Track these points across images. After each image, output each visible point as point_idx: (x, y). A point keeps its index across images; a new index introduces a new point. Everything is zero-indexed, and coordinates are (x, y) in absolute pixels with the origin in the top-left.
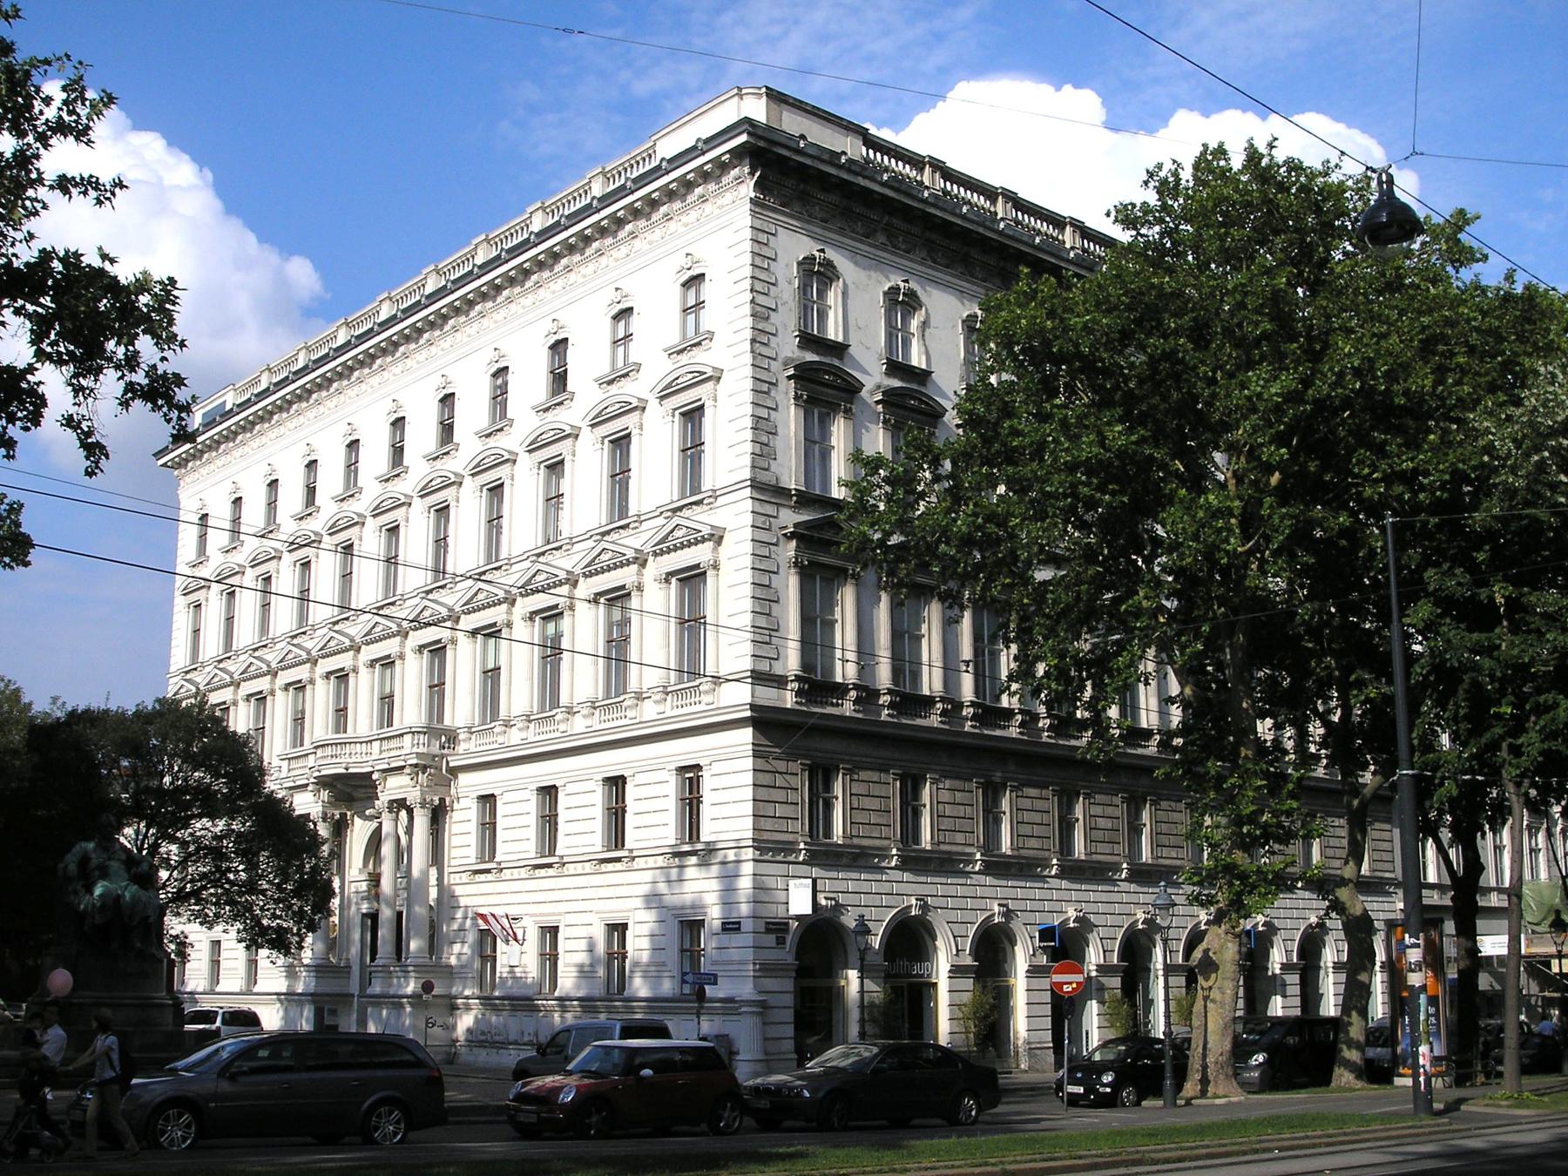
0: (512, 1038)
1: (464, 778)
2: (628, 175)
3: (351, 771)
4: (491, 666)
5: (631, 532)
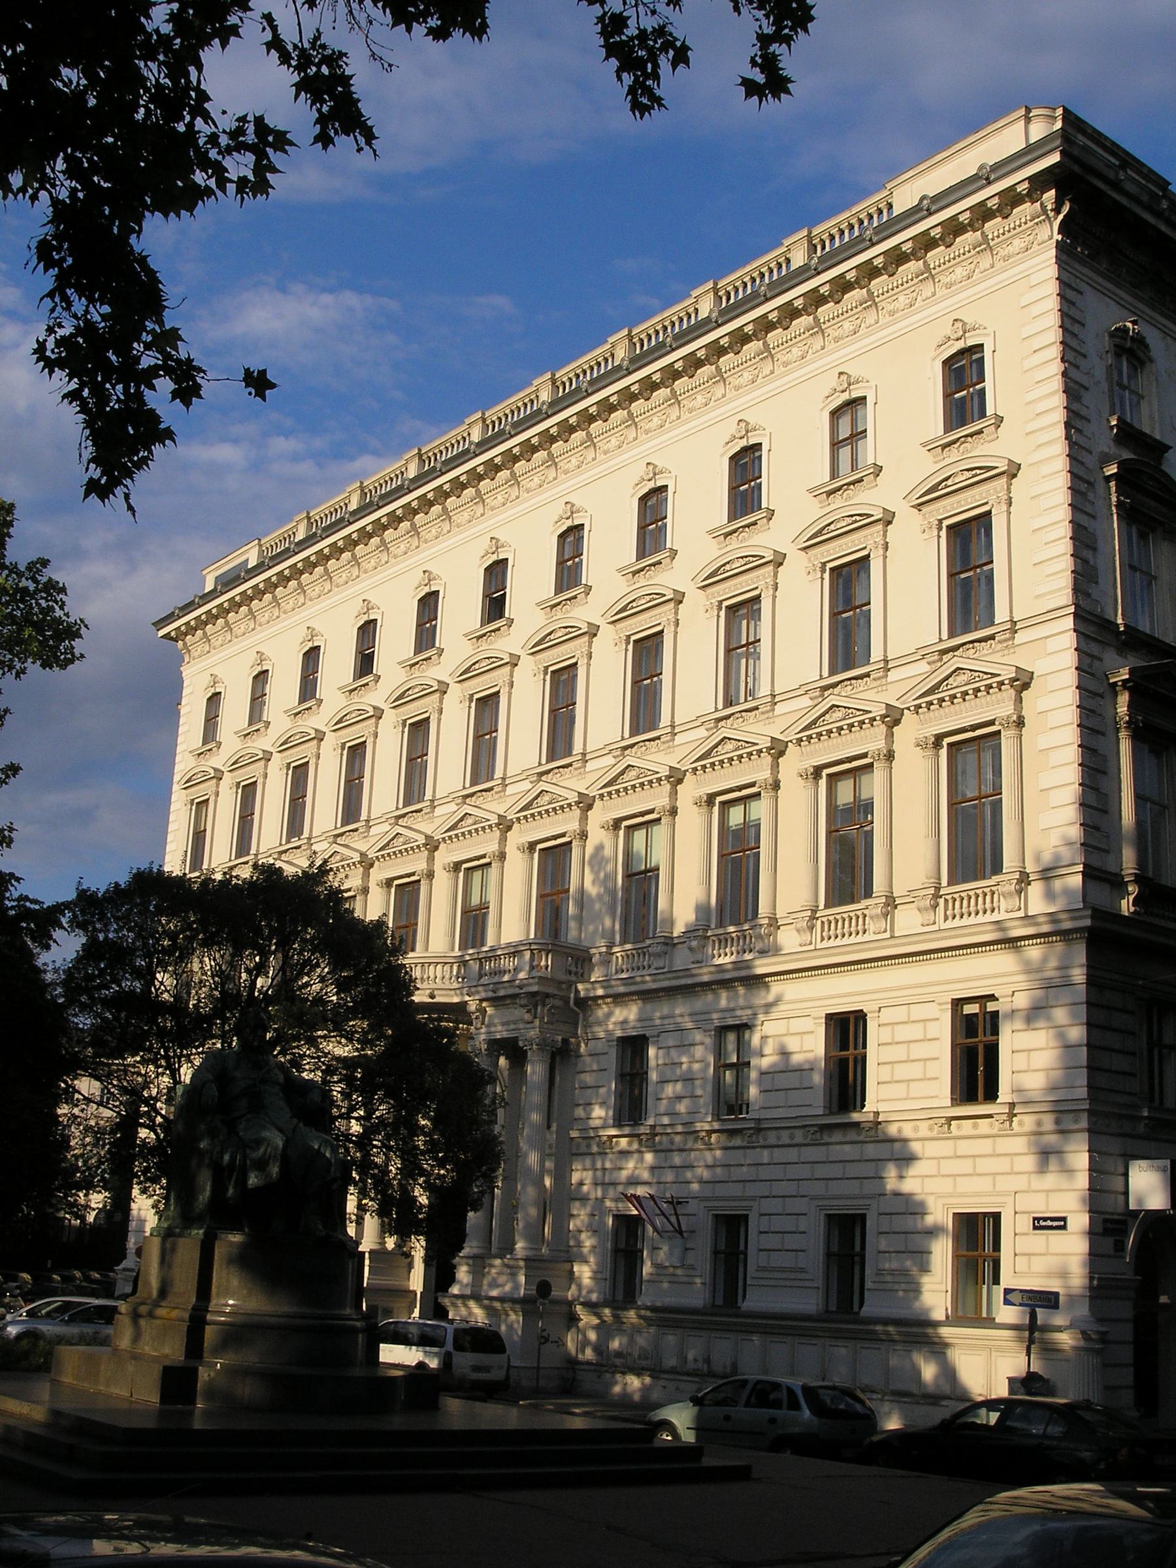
3: (438, 999)
4: (475, 900)
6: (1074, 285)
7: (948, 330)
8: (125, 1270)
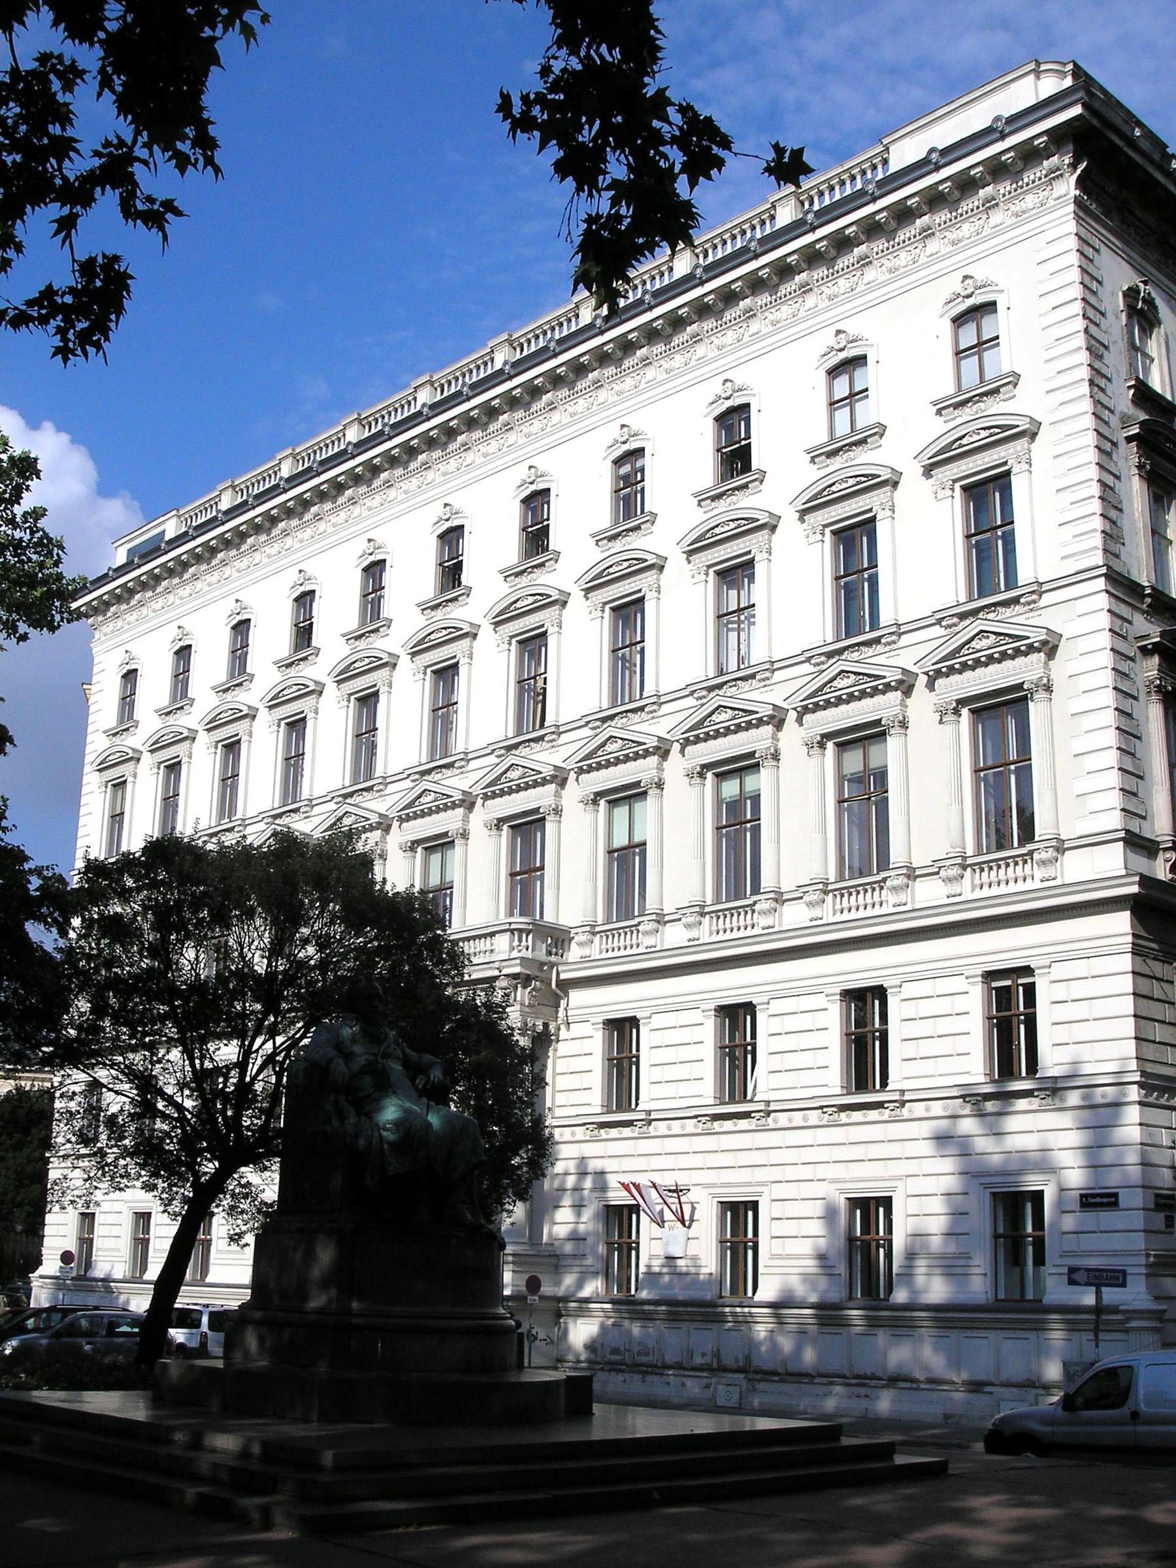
0: (671, 1357)
1: (577, 998)
2: (467, 379)
5: (456, 771)
6: (1091, 242)
7: (958, 287)
8: (42, 1277)
